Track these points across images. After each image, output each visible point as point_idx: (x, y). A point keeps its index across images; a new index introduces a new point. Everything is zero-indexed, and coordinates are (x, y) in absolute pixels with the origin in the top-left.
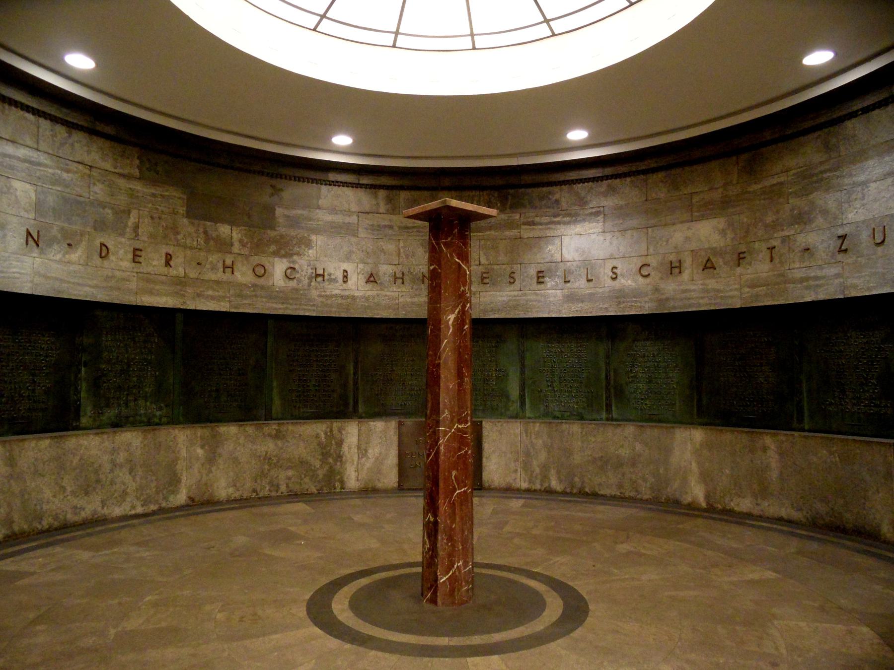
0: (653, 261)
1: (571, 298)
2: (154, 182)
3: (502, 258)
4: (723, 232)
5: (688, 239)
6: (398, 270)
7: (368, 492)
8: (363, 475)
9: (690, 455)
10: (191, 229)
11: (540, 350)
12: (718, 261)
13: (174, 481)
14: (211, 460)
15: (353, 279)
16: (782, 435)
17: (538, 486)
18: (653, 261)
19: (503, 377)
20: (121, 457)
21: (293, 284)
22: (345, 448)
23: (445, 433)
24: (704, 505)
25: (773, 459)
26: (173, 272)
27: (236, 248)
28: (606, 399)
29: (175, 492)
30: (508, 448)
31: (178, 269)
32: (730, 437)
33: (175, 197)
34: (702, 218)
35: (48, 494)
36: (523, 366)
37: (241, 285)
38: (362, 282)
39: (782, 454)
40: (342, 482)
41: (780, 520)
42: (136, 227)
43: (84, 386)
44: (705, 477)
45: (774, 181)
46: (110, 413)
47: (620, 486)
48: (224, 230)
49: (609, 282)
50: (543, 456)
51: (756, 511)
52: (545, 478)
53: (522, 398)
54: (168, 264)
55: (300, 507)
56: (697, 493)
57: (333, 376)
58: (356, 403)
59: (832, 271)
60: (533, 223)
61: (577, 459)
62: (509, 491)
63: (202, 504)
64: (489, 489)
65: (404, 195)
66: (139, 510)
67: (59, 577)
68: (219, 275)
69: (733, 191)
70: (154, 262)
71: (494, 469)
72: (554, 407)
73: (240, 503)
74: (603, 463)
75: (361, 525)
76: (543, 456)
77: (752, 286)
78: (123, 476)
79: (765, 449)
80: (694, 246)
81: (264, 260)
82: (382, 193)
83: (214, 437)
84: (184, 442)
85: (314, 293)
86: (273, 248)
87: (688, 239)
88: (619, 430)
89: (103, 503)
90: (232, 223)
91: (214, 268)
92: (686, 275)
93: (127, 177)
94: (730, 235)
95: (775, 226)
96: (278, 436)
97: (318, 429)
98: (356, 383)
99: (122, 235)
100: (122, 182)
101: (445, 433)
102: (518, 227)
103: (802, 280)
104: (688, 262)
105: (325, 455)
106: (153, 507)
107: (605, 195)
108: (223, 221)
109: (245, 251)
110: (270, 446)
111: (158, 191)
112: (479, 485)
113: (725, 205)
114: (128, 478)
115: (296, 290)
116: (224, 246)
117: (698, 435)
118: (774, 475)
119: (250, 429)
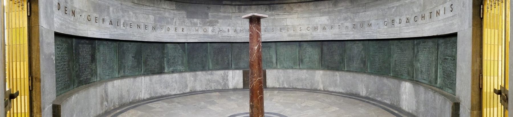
0: (310, 26)
1: (289, 35)
2: (179, 10)
3: (270, 24)
4: (328, 20)
5: (319, 21)
6: (242, 28)
7: (235, 90)
8: (234, 84)
9: (320, 77)
10: (188, 21)
11: (282, 50)
12: (327, 28)
13: (187, 86)
14: (195, 81)
15: (231, 31)
16: (340, 72)
17: (281, 87)
18: (310, 26)
19: (271, 58)
20: (174, 80)
21: (214, 33)
22: (229, 77)
23: (255, 81)
24: (323, 90)
25: (338, 78)
26: (184, 33)
27: (198, 25)
28: (299, 63)
29: (187, 89)
30: (273, 77)
31: (185, 32)
32: (329, 73)
33: (183, 13)
34: (322, 16)
35: (158, 88)
36: (276, 54)
37: (200, 35)
38: (233, 32)
39: (340, 77)
40: (228, 86)
41: (339, 93)
42: (175, 22)
43: (165, 62)
44: (323, 83)
45: (340, 8)
46: (171, 69)
47: (302, 86)
48: (195, 20)
49: (299, 32)
50: (282, 78)
51: (334, 91)
52: (283, 84)
53: (277, 63)
54: (183, 31)
55: (217, 93)
56: (321, 87)
57: (225, 58)
58: (232, 65)
59: (352, 33)
60: (279, 15)
61: (291, 79)
62: (274, 89)
63: (193, 93)
64: (269, 88)
65: (243, 7)
66: (178, 93)
67: (160, 110)
68: (195, 33)
69: (331, 9)
70: (180, 31)
71: (270, 83)
72: (285, 65)
73: (203, 92)
74: (298, 80)
75: (232, 100)
76: (282, 78)
77: (335, 35)
78: (174, 84)
79: (337, 75)
80: (320, 23)
81: (206, 27)
82: (237, 7)
83: (195, 75)
84: (188, 76)
85: (220, 36)
86: (208, 24)
87: (319, 21)
88: (302, 71)
89: (170, 91)
90: (197, 18)
91: (193, 31)
92: (319, 31)
93: (173, 10)
94: (329, 21)
95: (339, 20)
96: (211, 74)
97: (222, 72)
98: (231, 60)
99: (172, 25)
100: (172, 11)
101: (255, 81)
102: (274, 16)
103: (346, 34)
104: (319, 27)
105: (223, 79)
106: (182, 92)
107: (298, 7)
108: (195, 18)
109: (201, 25)
110: (209, 77)
111: (180, 12)
112: (266, 87)
113: (329, 13)
114: (175, 85)
115: (215, 35)
116: (195, 24)
117: (321, 72)
118: (338, 82)
119: (204, 72)
